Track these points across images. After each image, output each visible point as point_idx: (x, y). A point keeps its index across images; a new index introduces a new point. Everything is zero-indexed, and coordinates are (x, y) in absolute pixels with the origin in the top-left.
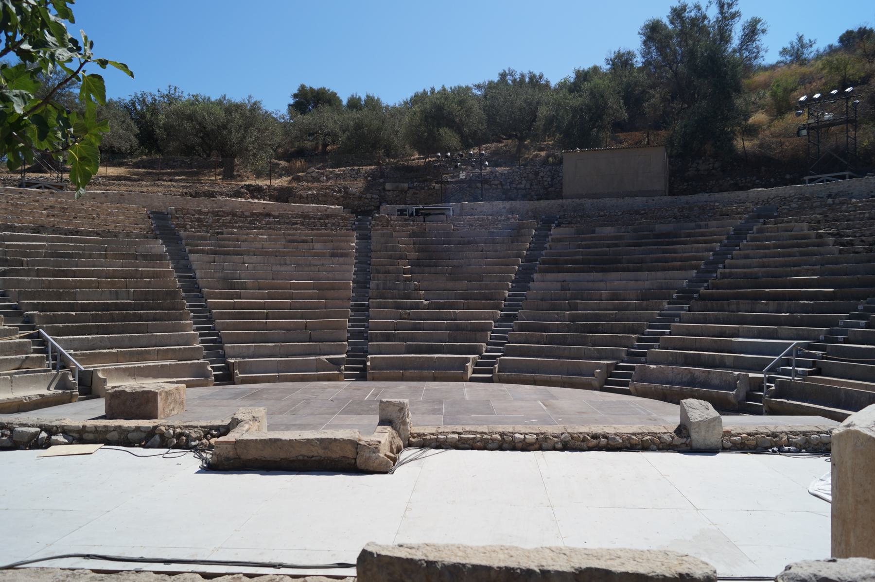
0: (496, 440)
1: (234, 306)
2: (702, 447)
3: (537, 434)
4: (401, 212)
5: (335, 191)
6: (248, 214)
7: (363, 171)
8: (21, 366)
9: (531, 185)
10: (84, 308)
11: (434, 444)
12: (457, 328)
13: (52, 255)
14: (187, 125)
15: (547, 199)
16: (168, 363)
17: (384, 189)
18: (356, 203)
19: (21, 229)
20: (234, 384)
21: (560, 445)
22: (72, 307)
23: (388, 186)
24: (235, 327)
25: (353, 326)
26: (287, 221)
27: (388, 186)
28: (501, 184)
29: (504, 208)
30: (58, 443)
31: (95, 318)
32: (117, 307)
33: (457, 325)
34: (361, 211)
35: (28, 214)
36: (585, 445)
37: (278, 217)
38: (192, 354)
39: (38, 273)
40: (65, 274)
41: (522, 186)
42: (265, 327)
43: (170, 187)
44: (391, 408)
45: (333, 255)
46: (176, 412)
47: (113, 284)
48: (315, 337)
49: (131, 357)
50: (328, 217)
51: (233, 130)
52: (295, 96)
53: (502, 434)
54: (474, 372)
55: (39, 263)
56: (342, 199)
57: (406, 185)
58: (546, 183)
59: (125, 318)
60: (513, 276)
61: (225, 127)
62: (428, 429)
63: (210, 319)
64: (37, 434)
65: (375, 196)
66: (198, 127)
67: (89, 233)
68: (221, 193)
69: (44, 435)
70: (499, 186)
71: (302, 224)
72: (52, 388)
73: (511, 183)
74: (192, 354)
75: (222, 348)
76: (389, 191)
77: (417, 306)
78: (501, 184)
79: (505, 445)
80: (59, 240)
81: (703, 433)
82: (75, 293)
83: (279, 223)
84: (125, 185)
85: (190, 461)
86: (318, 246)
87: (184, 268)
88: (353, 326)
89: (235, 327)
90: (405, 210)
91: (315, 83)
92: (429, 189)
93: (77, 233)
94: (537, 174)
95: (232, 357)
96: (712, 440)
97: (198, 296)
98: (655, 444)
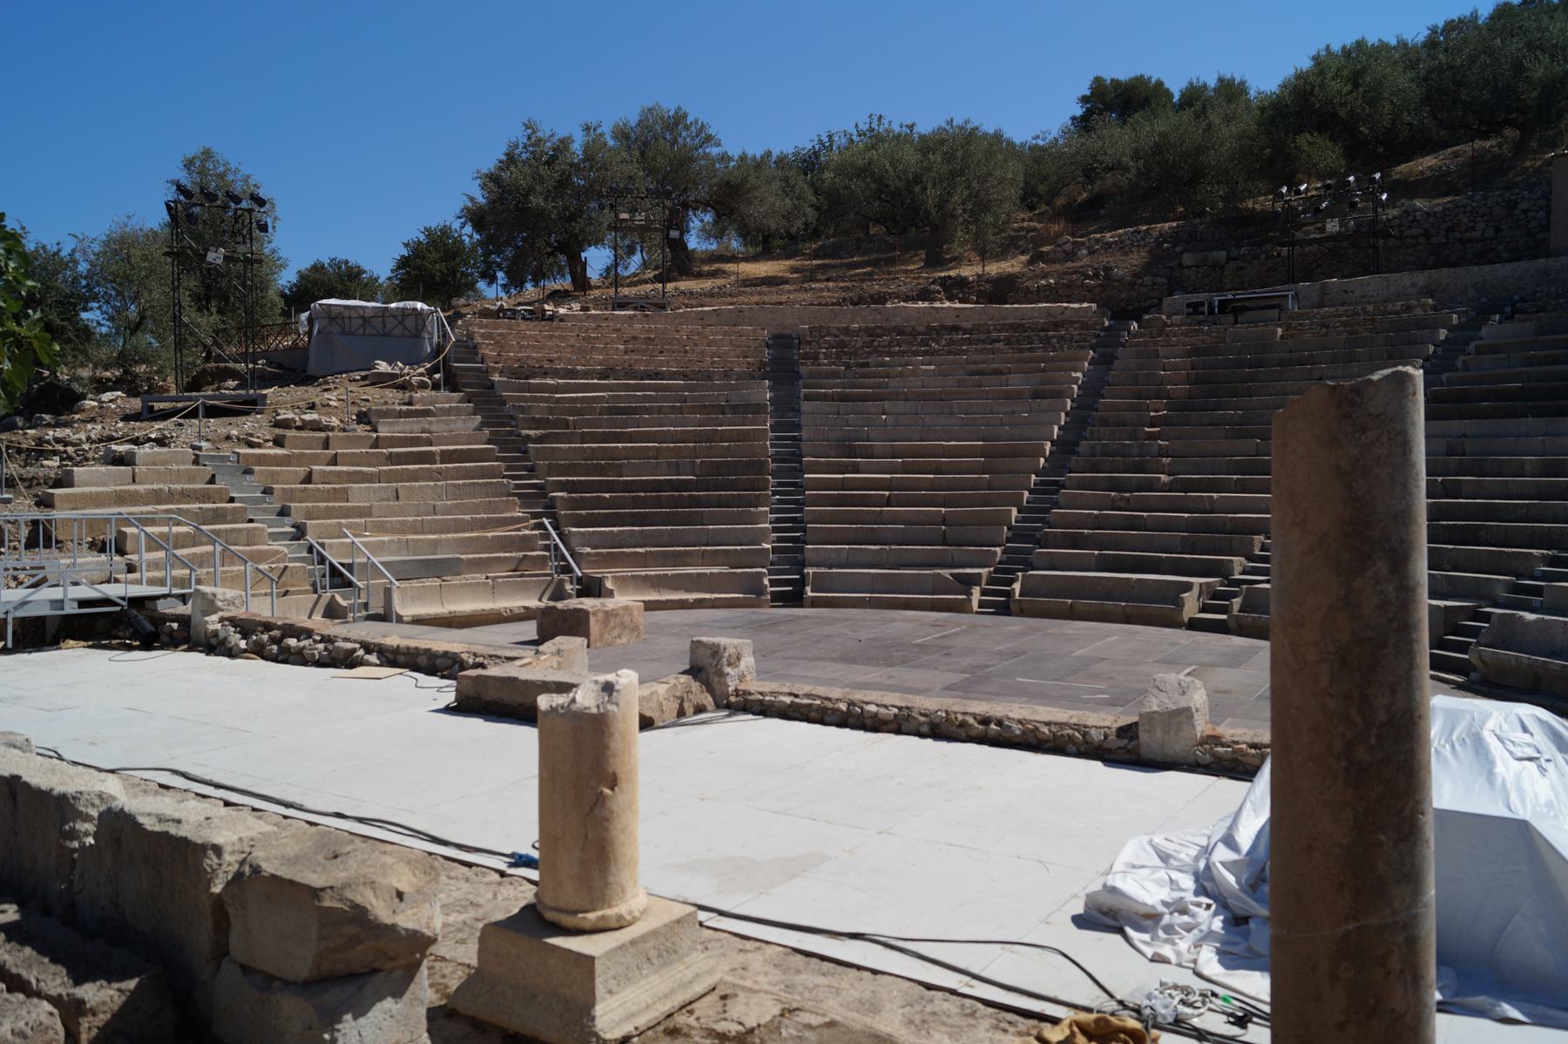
0: (839, 710)
1: (842, 485)
2: (1159, 759)
3: (900, 708)
4: (1195, 308)
5: (1088, 277)
6: (922, 329)
7: (1155, 234)
8: (518, 567)
9: (1498, 230)
10: (628, 487)
11: (757, 708)
12: (1208, 527)
13: (609, 411)
14: (856, 185)
15: (1534, 257)
16: (716, 570)
17: (1180, 265)
18: (1124, 295)
19: (585, 375)
20: (802, 606)
21: (925, 729)
22: (610, 487)
23: (1187, 259)
24: (833, 518)
25: (1024, 520)
26: (982, 337)
27: (1187, 259)
28: (1427, 235)
29: (1413, 285)
30: (369, 664)
31: (636, 503)
32: (672, 486)
33: (1206, 520)
34: (1125, 304)
35: (600, 351)
36: (962, 733)
37: (970, 331)
38: (756, 558)
39: (584, 438)
40: (618, 438)
41: (1476, 234)
42: (880, 518)
43: (822, 290)
44: (701, 650)
45: (1037, 395)
46: (624, 640)
47: (677, 451)
48: (955, 537)
49: (665, 559)
50: (1056, 326)
51: (930, 185)
52: (1084, 100)
53: (851, 704)
54: (1204, 609)
55: (589, 424)
56: (1098, 290)
57: (1223, 254)
58: (1533, 224)
59: (678, 503)
60: (1048, 446)
61: (917, 180)
62: (757, 686)
63: (800, 505)
64: (354, 650)
65: (1159, 280)
66: (873, 186)
67: (673, 376)
68: (907, 296)
69: (361, 652)
70: (1421, 240)
71: (1008, 341)
72: (545, 600)
73: (1450, 230)
74: (756, 558)
75: (801, 550)
76: (1189, 267)
77: (1150, 486)
78: (1427, 235)
79: (851, 721)
80: (627, 387)
81: (1159, 734)
82: (620, 466)
83: (969, 342)
84: (759, 293)
85: (444, 691)
86: (1016, 382)
87: (788, 424)
88: (1024, 520)
89: (833, 518)
90: (1202, 304)
91: (1120, 70)
92: (1268, 258)
93: (657, 375)
94: (1512, 205)
95: (812, 565)
96: (1178, 748)
97: (795, 469)
98: (1075, 744)
